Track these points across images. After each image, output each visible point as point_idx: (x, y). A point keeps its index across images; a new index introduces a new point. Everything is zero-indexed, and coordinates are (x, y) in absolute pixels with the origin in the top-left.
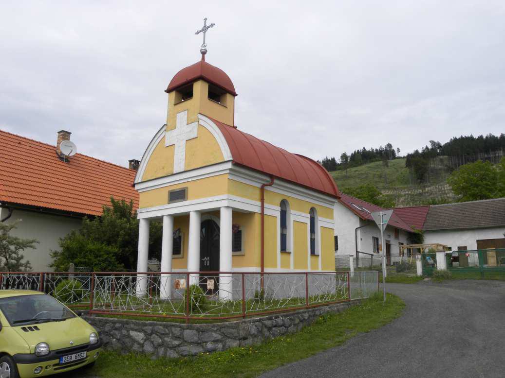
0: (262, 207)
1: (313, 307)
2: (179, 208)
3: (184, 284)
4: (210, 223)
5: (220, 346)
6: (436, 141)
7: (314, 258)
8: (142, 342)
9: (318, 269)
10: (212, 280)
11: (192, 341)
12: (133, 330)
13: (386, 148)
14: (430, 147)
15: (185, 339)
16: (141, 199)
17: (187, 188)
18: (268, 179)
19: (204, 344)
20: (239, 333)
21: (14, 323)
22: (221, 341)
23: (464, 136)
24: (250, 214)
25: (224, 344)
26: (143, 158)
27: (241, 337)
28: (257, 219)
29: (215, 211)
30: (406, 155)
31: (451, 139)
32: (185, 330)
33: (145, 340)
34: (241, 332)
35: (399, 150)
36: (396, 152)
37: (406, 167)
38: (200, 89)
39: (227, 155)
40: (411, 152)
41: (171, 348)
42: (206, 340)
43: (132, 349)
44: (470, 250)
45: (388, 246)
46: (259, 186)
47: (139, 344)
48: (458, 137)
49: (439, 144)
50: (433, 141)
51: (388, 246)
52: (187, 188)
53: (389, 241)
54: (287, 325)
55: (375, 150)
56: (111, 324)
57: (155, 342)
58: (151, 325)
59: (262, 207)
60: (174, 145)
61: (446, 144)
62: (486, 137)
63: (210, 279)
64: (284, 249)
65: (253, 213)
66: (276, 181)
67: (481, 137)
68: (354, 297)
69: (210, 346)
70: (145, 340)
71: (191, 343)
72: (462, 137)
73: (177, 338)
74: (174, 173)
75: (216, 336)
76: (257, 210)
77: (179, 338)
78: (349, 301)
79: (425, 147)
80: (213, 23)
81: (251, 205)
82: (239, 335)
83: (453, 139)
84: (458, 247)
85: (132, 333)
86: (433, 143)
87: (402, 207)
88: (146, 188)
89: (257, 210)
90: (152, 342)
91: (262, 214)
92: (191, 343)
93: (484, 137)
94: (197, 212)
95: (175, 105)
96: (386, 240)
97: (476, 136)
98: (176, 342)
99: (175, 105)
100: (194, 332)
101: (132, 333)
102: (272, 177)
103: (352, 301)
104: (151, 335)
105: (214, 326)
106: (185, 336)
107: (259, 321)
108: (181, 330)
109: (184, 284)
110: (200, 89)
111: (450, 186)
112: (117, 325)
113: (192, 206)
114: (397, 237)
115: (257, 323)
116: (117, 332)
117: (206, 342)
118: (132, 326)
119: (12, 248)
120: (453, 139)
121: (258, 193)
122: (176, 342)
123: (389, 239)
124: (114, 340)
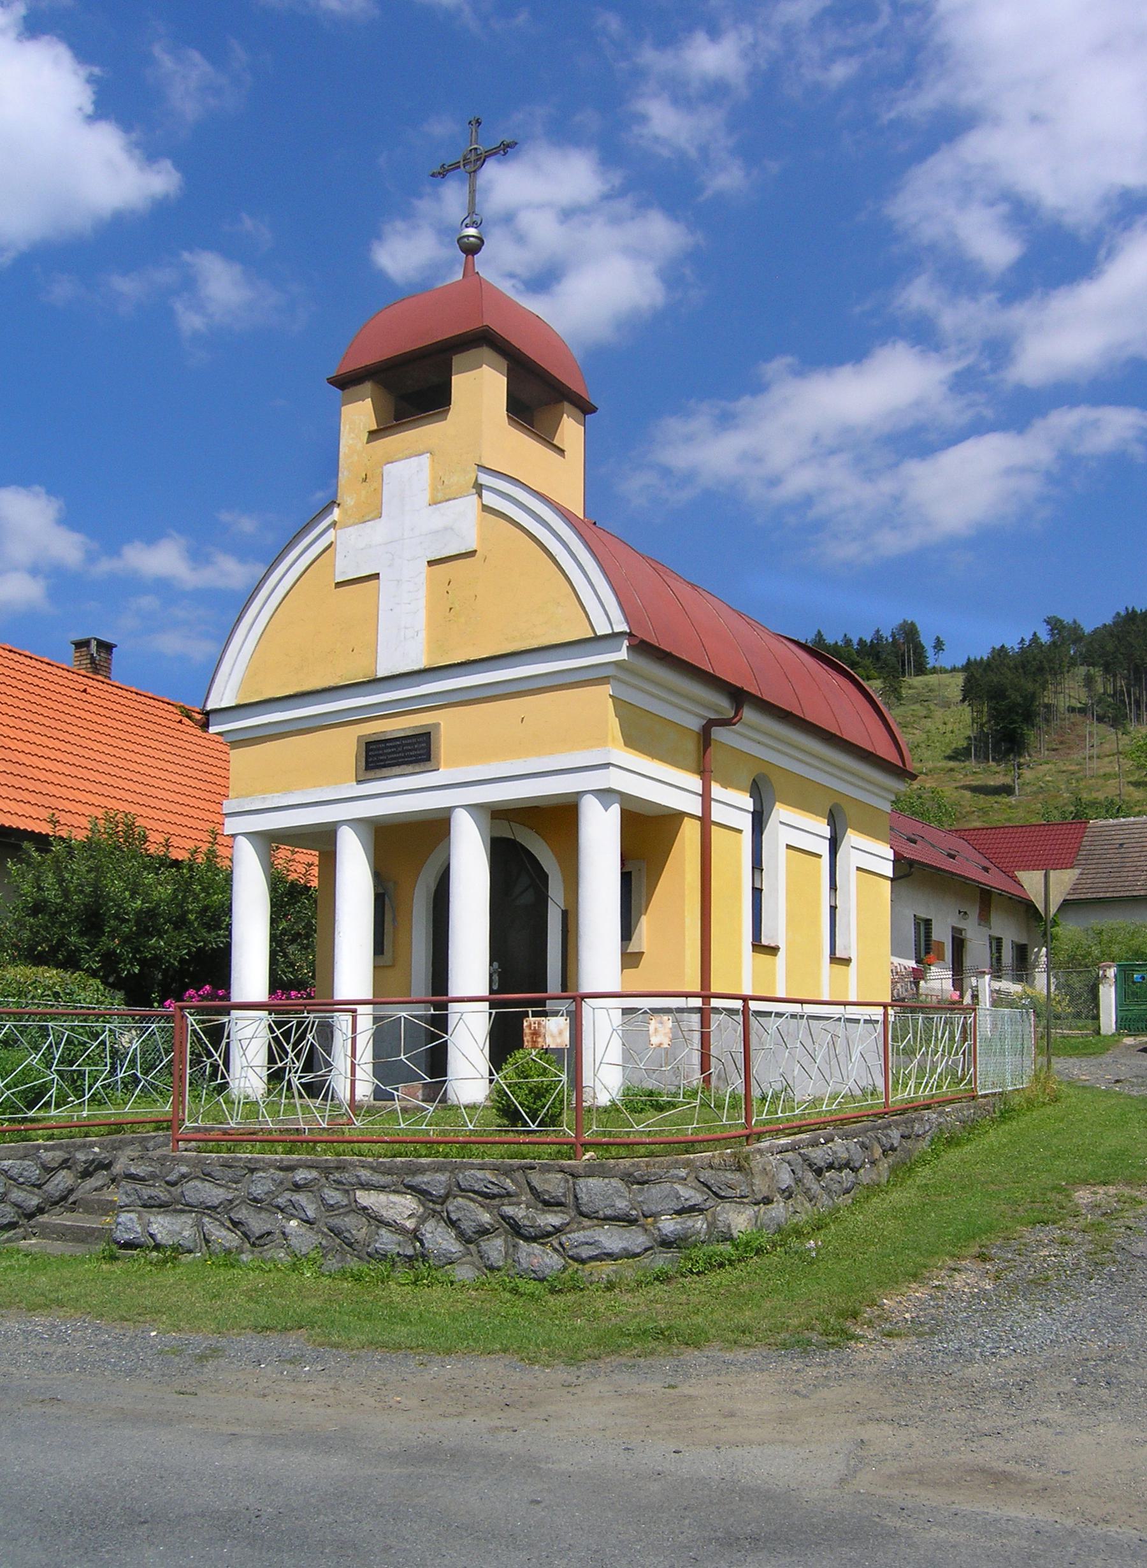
0: (706, 798)
1: (904, 1111)
2: (402, 795)
3: (561, 1033)
4: (530, 847)
5: (699, 1223)
6: (1067, 620)
7: (838, 968)
8: (410, 1224)
11: (609, 1212)
12: (366, 1186)
13: (893, 635)
14: (1045, 638)
15: (584, 1209)
16: (232, 766)
17: (437, 726)
18: (724, 705)
19: (650, 1220)
20: (752, 1185)
22: (701, 1211)
24: (672, 819)
25: (710, 1219)
27: (759, 1197)
28: (690, 832)
29: (410, 823)
30: (961, 662)
31: (1118, 614)
32: (581, 1180)
33: (423, 1220)
34: (756, 1181)
35: (939, 645)
36: (930, 652)
37: (963, 701)
38: (481, 388)
39: (608, 616)
40: (982, 653)
41: (530, 1239)
42: (654, 1209)
43: (573, 1214)
45: (959, 944)
46: (695, 724)
47: (401, 1230)
49: (1076, 628)
50: (1058, 620)
51: (959, 944)
52: (437, 726)
53: (960, 931)
54: (857, 1165)
55: (855, 642)
56: (272, 1171)
57: (464, 1225)
58: (439, 1169)
59: (706, 798)
60: (376, 576)
61: (1095, 632)
65: (680, 815)
66: (749, 714)
68: (984, 1087)
69: (669, 1225)
70: (423, 1220)
71: (606, 1219)
73: (550, 1204)
74: (380, 675)
75: (690, 1195)
76: (693, 806)
77: (560, 1204)
78: (974, 1098)
79: (1028, 638)
80: (508, 140)
81: (669, 786)
82: (572, 1219)
83: (1123, 613)
85: (365, 1198)
86: (1055, 625)
87: (978, 824)
89: (693, 806)
90: (452, 1223)
91: (705, 821)
92: (606, 1219)
94: (474, 809)
96: (953, 928)
98: (553, 1219)
100: (616, 1182)
101: (365, 1198)
102: (739, 697)
103: (985, 1096)
104: (444, 1199)
105: (676, 1165)
106: (584, 1198)
107: (793, 1148)
108: (567, 1181)
109: (561, 1033)
110: (481, 388)
111: (109, 893)
112: (301, 1175)
113: (465, 784)
114: (984, 917)
115: (790, 1155)
116: (301, 1198)
117: (655, 1215)
118: (365, 1174)
120: (1123, 613)
121: (691, 746)
122: (553, 1219)
123: (960, 926)
124: (294, 1223)
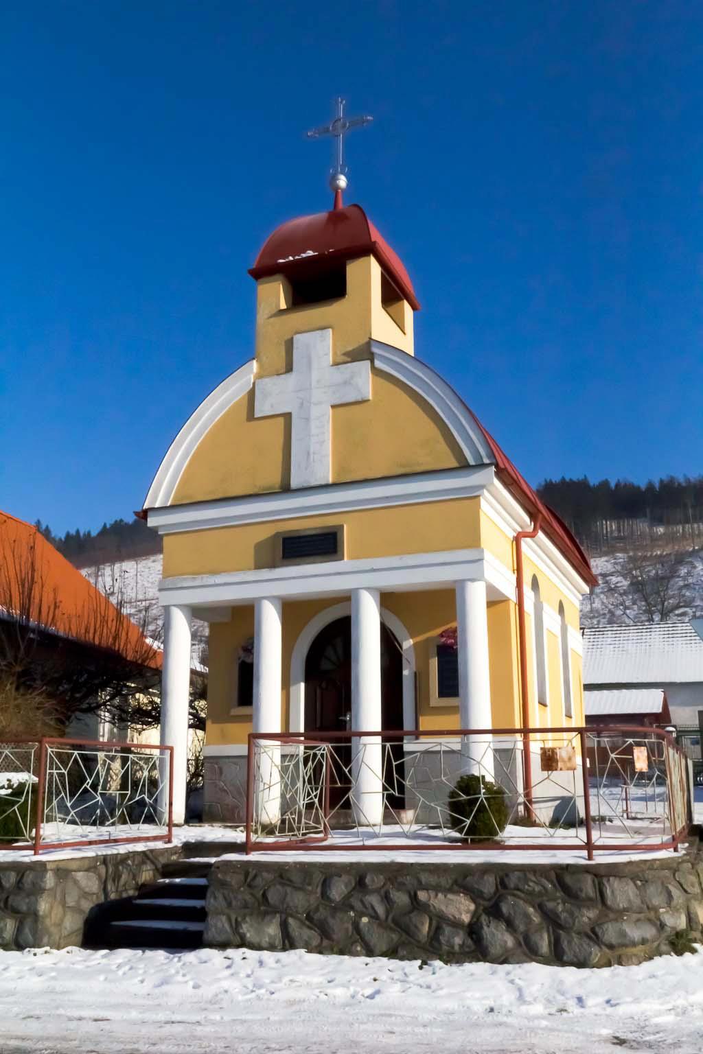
9: (395, 761)
10: (643, 748)
21: (332, 829)
23: (567, 479)
26: (492, 507)
31: (540, 484)
44: (538, 726)
48: (556, 479)
62: (617, 485)
63: (639, 744)
64: (543, 703)
67: (605, 484)
72: (563, 479)
83: (543, 483)
84: (587, 717)
88: (556, 575)
93: (613, 485)
95: (336, 364)
97: (594, 481)
99: (336, 364)
119: (68, 705)
